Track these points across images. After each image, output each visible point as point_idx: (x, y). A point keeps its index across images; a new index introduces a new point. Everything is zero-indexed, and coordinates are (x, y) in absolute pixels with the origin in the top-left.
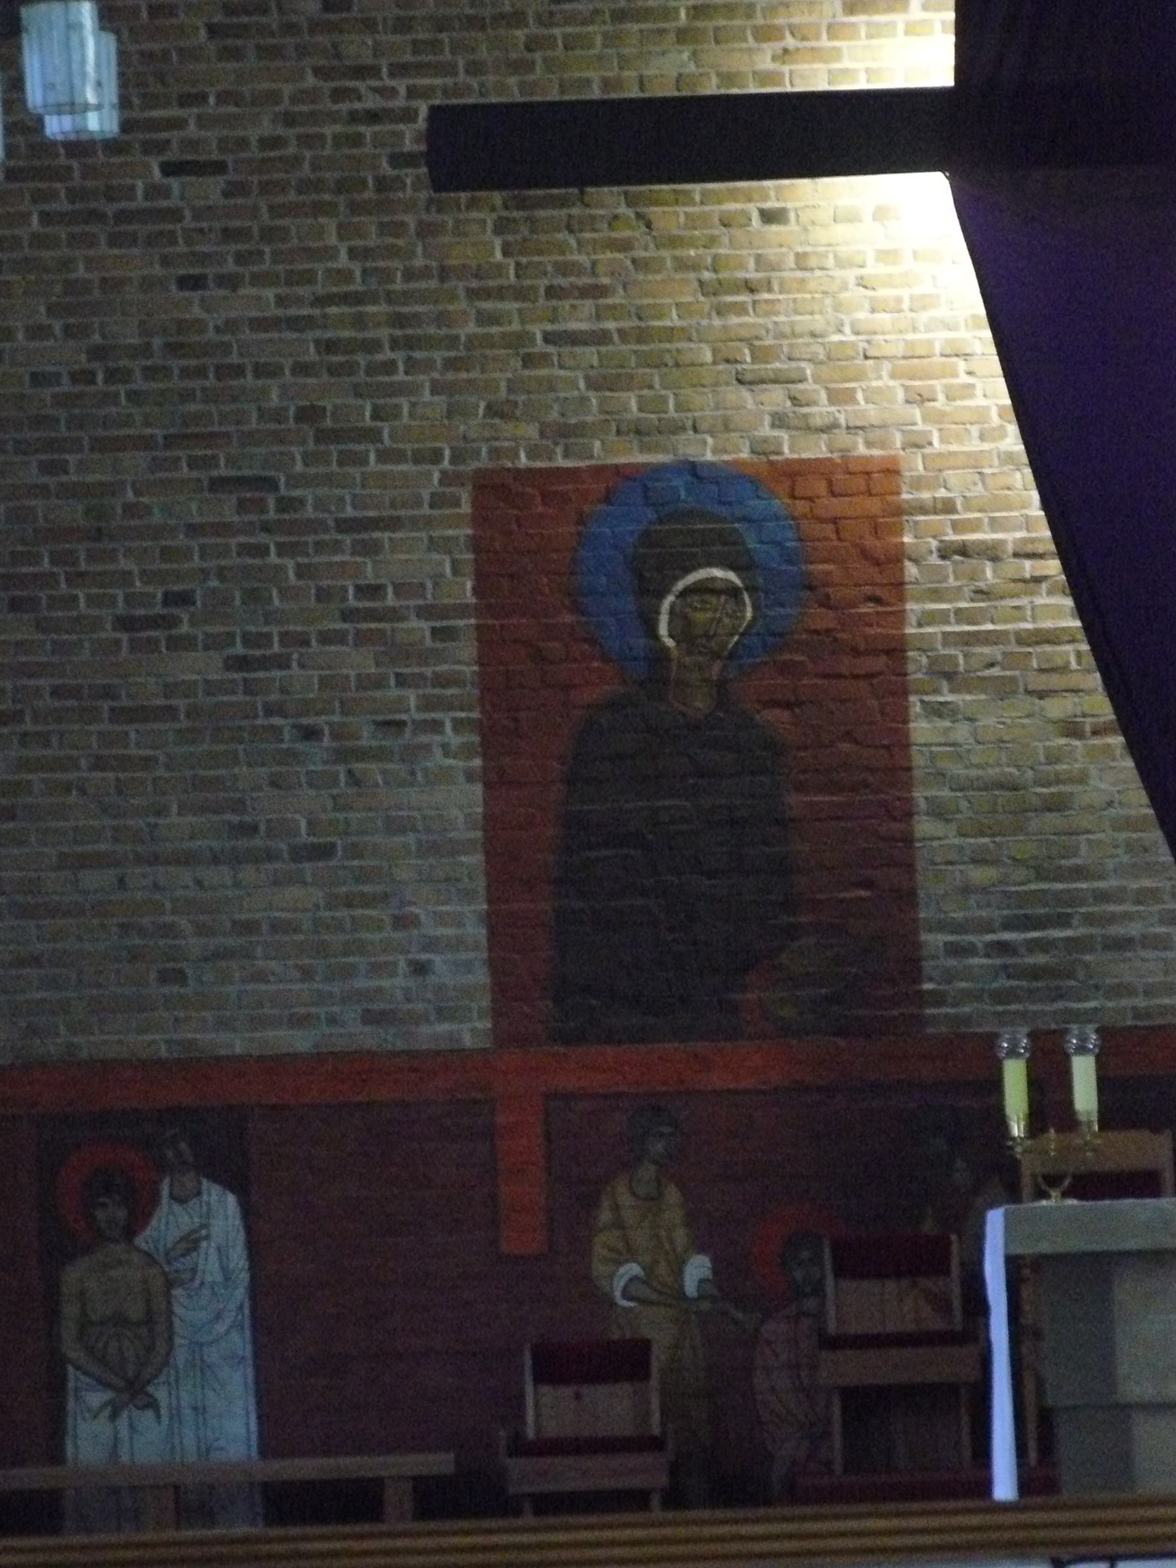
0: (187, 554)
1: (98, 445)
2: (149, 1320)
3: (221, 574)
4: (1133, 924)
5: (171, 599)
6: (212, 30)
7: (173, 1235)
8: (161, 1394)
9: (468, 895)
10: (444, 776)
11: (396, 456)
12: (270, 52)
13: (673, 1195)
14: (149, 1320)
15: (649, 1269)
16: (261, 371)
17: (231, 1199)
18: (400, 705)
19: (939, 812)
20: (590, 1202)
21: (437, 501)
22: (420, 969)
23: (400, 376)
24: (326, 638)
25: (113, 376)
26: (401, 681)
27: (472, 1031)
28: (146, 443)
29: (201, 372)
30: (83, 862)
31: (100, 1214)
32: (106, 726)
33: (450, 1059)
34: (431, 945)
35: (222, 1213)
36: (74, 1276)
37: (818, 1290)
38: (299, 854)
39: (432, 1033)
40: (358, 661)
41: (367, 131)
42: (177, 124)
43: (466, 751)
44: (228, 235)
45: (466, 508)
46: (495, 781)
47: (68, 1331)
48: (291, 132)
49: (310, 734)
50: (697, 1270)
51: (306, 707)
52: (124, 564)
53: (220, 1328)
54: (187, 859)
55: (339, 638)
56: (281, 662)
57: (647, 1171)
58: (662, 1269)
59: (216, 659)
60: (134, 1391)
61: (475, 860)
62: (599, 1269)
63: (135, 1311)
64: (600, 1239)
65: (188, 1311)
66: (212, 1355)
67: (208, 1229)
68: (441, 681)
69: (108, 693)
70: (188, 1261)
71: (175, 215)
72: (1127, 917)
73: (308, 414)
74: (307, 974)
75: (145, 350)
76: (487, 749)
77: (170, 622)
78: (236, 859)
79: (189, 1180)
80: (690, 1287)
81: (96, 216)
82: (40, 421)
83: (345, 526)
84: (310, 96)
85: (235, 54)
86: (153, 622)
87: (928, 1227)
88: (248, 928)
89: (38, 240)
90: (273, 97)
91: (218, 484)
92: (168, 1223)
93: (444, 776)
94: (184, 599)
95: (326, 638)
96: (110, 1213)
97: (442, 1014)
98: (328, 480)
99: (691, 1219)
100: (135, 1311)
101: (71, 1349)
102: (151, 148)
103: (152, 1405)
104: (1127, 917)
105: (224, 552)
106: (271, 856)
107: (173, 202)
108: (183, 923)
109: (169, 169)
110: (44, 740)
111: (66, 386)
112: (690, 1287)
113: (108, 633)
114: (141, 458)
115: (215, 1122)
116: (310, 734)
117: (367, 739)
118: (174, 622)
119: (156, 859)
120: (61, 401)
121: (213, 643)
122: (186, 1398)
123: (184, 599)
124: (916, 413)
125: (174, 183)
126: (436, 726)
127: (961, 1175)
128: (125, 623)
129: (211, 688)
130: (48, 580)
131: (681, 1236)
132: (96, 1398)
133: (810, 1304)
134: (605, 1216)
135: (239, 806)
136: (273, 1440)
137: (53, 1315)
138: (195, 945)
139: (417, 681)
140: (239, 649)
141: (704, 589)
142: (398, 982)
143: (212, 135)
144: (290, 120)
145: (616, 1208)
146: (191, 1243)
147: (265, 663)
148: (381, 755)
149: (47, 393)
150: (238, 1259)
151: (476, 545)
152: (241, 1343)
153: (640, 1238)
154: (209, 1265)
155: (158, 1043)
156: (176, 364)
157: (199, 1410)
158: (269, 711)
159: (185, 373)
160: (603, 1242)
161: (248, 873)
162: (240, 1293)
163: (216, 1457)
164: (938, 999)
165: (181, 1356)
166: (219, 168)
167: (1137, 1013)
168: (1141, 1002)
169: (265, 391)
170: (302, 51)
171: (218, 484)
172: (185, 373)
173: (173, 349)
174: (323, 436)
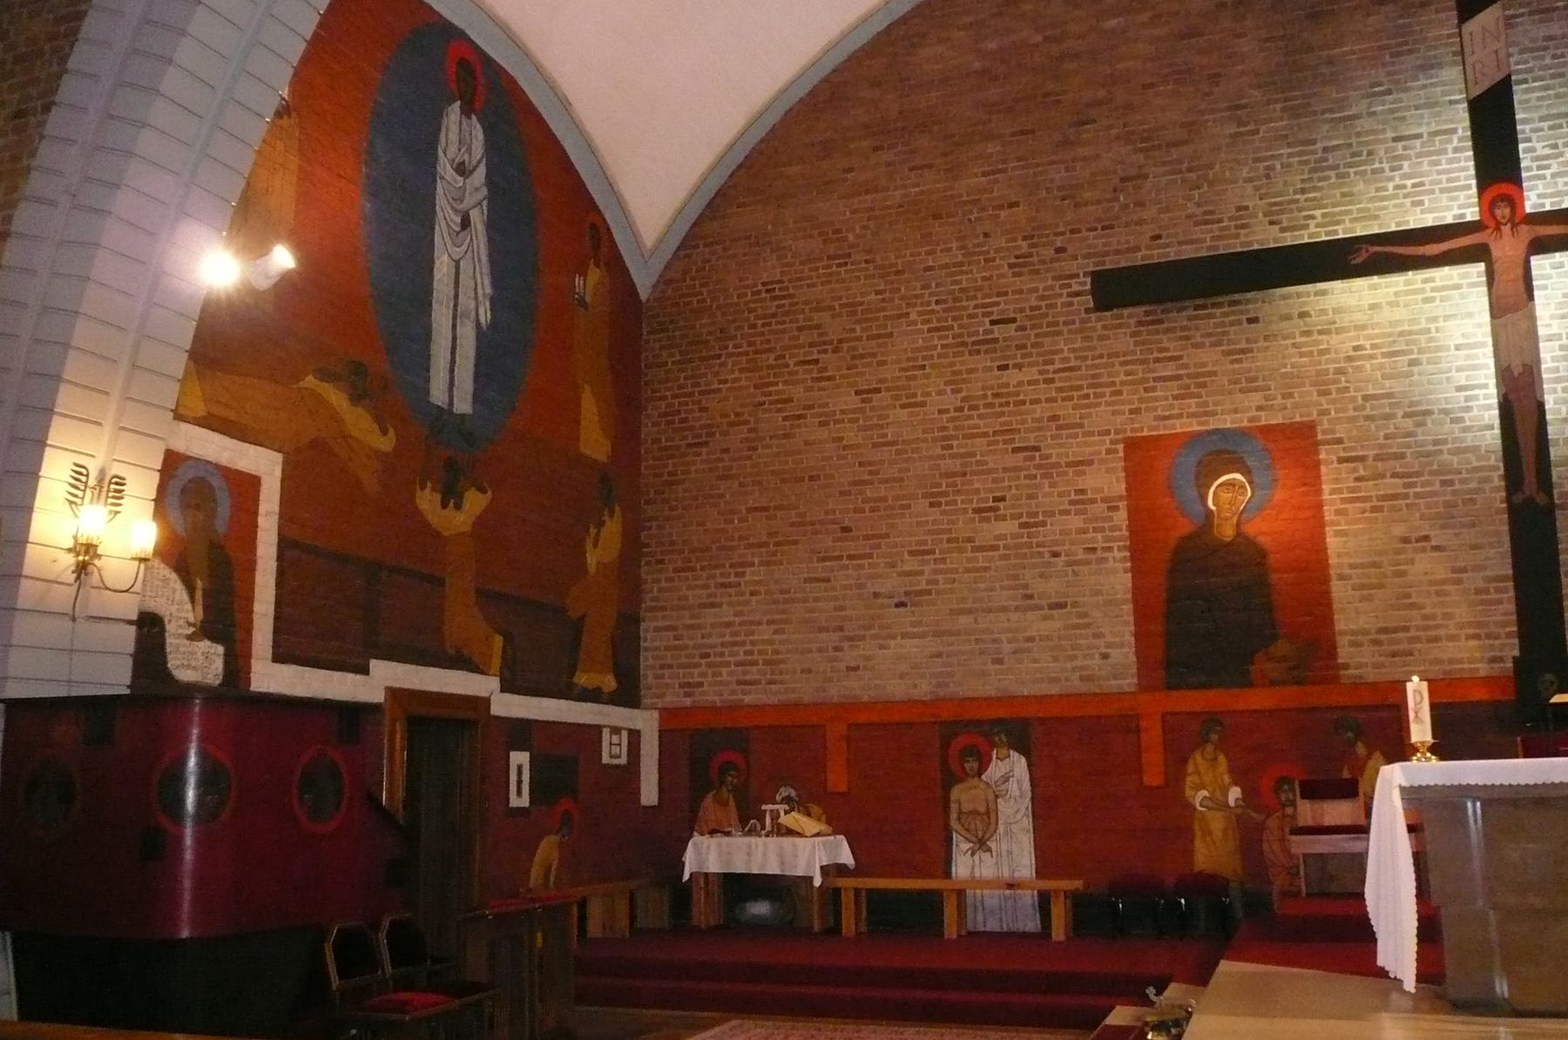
0: (1003, 480)
1: (965, 437)
2: (988, 813)
3: (1017, 487)
4: (1444, 73)
5: (996, 499)
6: (1011, 266)
7: (998, 775)
8: (992, 845)
9: (1127, 623)
10: (1115, 571)
11: (1092, 434)
12: (1037, 272)
13: (1222, 759)
14: (988, 813)
15: (1212, 793)
16: (1033, 402)
17: (1023, 760)
18: (1094, 540)
19: (1341, 577)
20: (1185, 761)
21: (1109, 452)
22: (1105, 656)
23: (1092, 400)
24: (1062, 513)
25: (971, 408)
26: (1095, 530)
27: (1129, 683)
28: (986, 435)
29: (1008, 404)
30: (960, 612)
31: (967, 765)
32: (969, 554)
33: (1121, 695)
34: (1109, 645)
35: (1018, 765)
36: (956, 792)
37: (1293, 804)
38: (1052, 607)
39: (1113, 685)
40: (1075, 522)
41: (1076, 300)
42: (998, 304)
43: (1124, 559)
44: (1018, 347)
45: (1121, 454)
46: (1137, 572)
47: (954, 816)
48: (1043, 304)
49: (1056, 555)
50: (1235, 793)
51: (1056, 543)
52: (976, 486)
53: (1019, 816)
54: (1004, 609)
55: (1067, 512)
56: (1044, 524)
57: (1209, 748)
58: (1218, 793)
59: (1016, 523)
60: (981, 844)
61: (1128, 607)
62: (1188, 792)
63: (982, 809)
64: (1189, 779)
65: (1005, 808)
66: (1014, 828)
67: (1011, 773)
68: (1112, 529)
69: (970, 540)
70: (1003, 787)
71: (996, 340)
72: (1438, 627)
73: (1054, 418)
74: (1056, 659)
75: (985, 396)
76: (1133, 558)
77: (996, 509)
78: (1025, 609)
79: (1004, 751)
80: (1232, 803)
81: (964, 344)
82: (944, 428)
83: (850, 557)
84: (1052, 288)
85: (1019, 274)
86: (991, 509)
87: (1346, 774)
88: (1030, 639)
89: (940, 356)
90: (1036, 290)
91: (1015, 450)
92: (995, 770)
93: (1115, 571)
94: (1003, 499)
95: (1062, 513)
96: (971, 765)
97: (1115, 677)
98: (1061, 446)
99: (1231, 771)
100: (982, 809)
101: (954, 823)
102: (985, 315)
103: (989, 850)
104: (1438, 627)
105: (1019, 478)
106: (1040, 608)
107: (996, 335)
108: (1003, 637)
109: (993, 323)
110: (944, 560)
111: (952, 414)
112: (1232, 803)
113: (970, 515)
114: (984, 441)
115: (1018, 726)
116: (1056, 555)
117: (1081, 556)
118: (998, 509)
119: (990, 611)
120: (953, 419)
121: (1013, 517)
122: (1004, 848)
123: (1003, 499)
124: (1323, 400)
125: (995, 327)
126: (1110, 549)
127: (1361, 749)
128: (977, 511)
129: (1014, 536)
130: (945, 494)
131: (1227, 779)
132: (965, 846)
133: (1289, 811)
134: (1190, 768)
135: (1026, 586)
136: (1041, 872)
137: (947, 807)
138: (1007, 647)
139: (1102, 530)
140: (1024, 519)
141: (1230, 484)
142: (1097, 661)
143: (1012, 307)
144: (1042, 298)
145: (1196, 766)
146: (1006, 779)
147: (1036, 525)
148: (1088, 563)
149: (945, 416)
150: (1027, 785)
151: (1126, 469)
152: (1028, 823)
153: (1207, 778)
154: (1013, 787)
155: (989, 689)
156: (997, 401)
157: (1010, 853)
158: (1038, 545)
159: (1001, 405)
160: (1190, 780)
161: (1029, 615)
162: (1027, 801)
163: (1016, 874)
164: (1346, 666)
165: (1001, 829)
166: (1013, 320)
167: (1445, 672)
168: (1448, 668)
169: (1034, 411)
170: (1047, 271)
171: (1015, 450)
172: (1001, 405)
173: (996, 395)
174: (1059, 428)
